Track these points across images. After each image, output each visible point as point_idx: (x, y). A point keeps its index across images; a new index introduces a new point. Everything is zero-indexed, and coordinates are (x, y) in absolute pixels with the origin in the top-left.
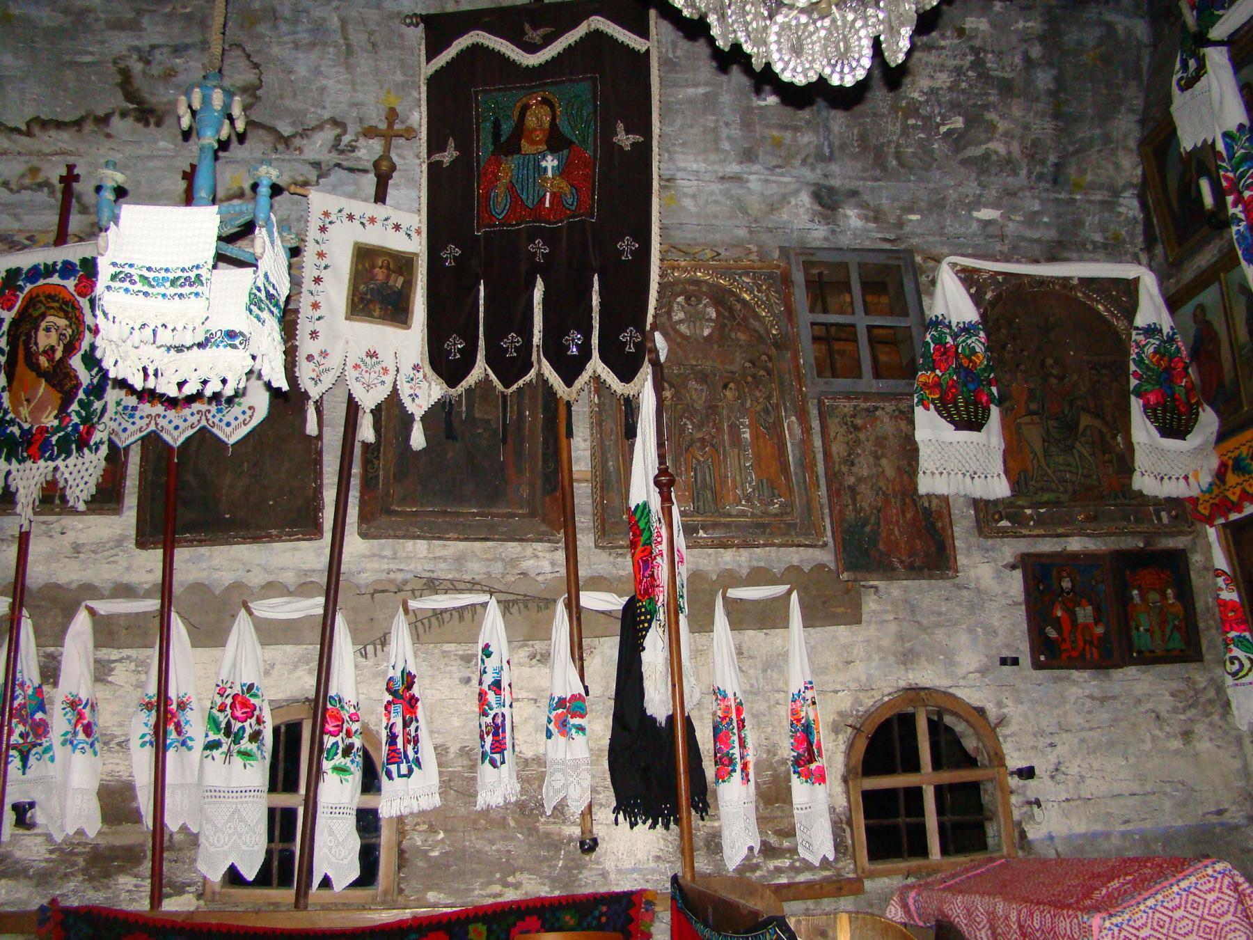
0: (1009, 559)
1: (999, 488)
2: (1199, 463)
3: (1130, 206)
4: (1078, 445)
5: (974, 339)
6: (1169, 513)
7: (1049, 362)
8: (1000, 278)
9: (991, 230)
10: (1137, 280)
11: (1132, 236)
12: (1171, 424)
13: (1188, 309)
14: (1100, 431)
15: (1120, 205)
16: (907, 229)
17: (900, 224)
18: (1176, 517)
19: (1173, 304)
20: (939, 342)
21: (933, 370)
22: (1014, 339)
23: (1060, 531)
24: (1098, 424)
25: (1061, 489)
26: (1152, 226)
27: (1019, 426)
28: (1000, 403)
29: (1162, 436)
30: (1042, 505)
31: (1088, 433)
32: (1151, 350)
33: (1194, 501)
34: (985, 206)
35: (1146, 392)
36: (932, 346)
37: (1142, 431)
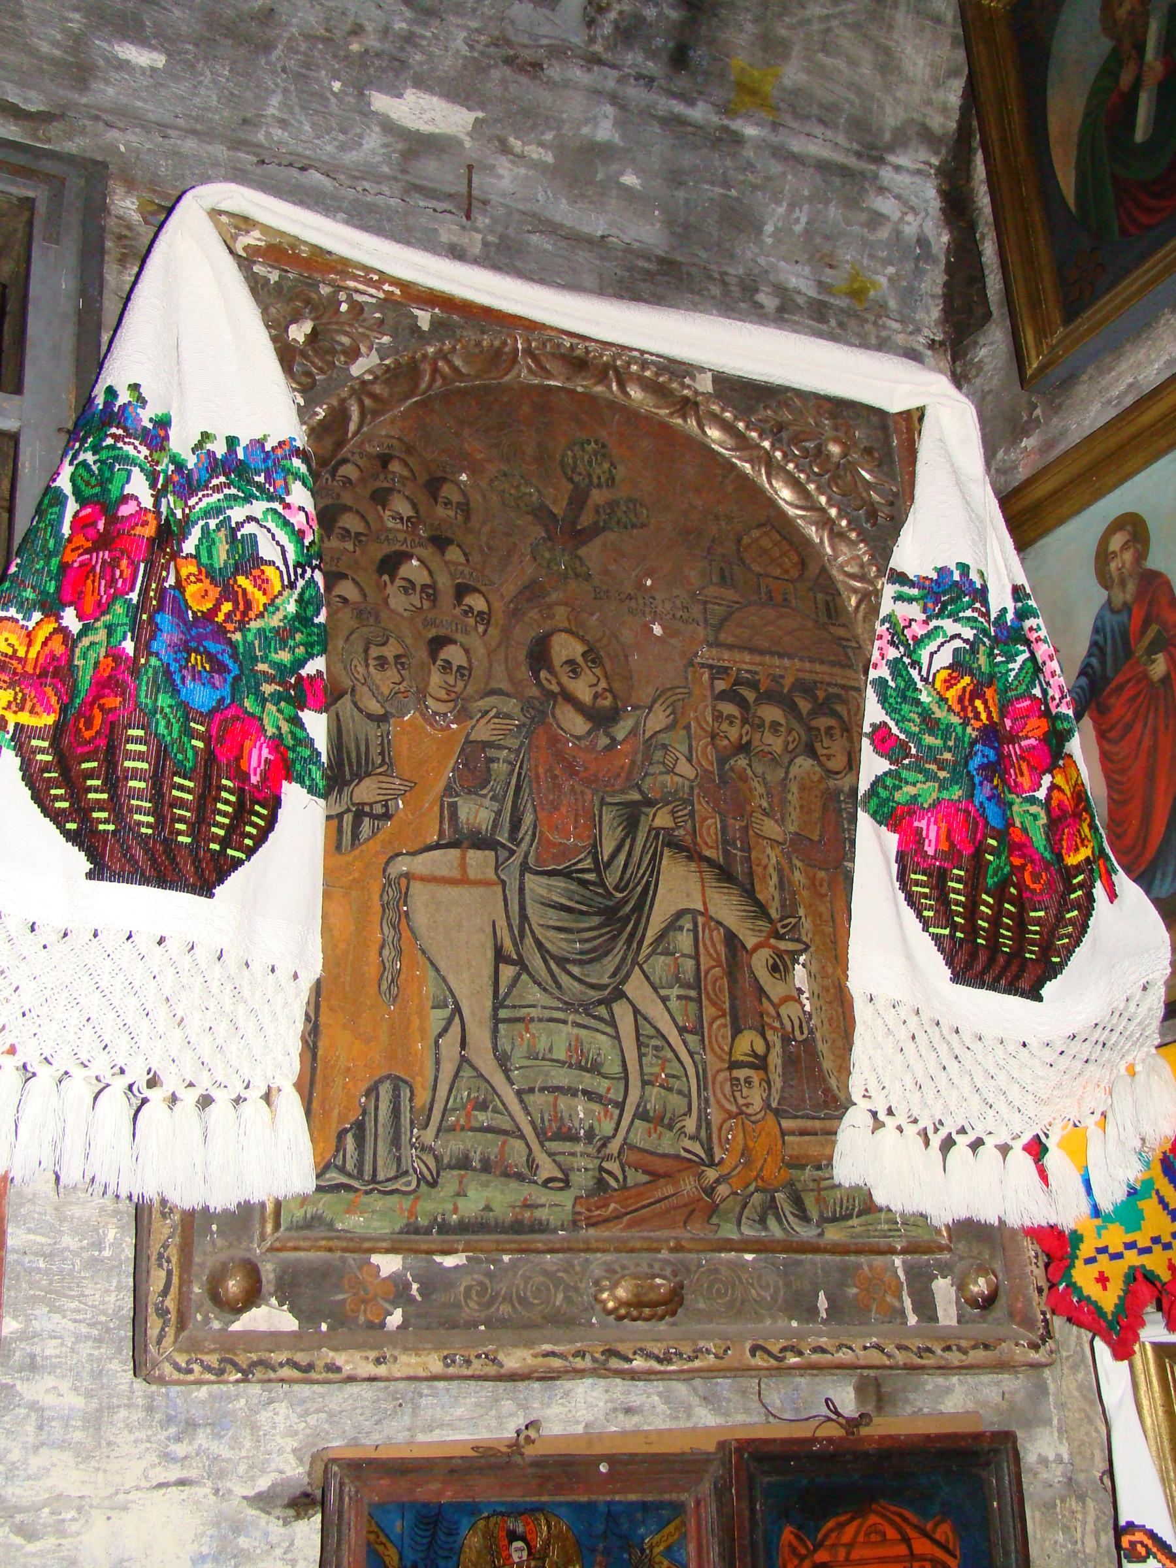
0: (293, 1470)
1: (268, 1157)
2: (1096, 1100)
3: (909, 196)
4: (636, 987)
5: (259, 508)
6: (961, 1287)
7: (565, 648)
8: (424, 318)
9: (429, 169)
10: (913, 419)
11: (909, 296)
12: (993, 936)
13: (1078, 535)
14: (731, 939)
15: (882, 190)
16: (106, 92)
17: (80, 70)
18: (988, 1302)
19: (1027, 515)
20: (100, 501)
21: (51, 609)
22: (440, 542)
23: (514, 1359)
24: (727, 909)
25: (547, 1169)
26: (977, 278)
27: (398, 892)
28: (336, 779)
29: (957, 978)
30: (452, 1231)
31: (684, 941)
32: (944, 658)
33: (1057, 1246)
34: (421, 83)
35: (912, 809)
36: (72, 507)
37: (889, 948)
